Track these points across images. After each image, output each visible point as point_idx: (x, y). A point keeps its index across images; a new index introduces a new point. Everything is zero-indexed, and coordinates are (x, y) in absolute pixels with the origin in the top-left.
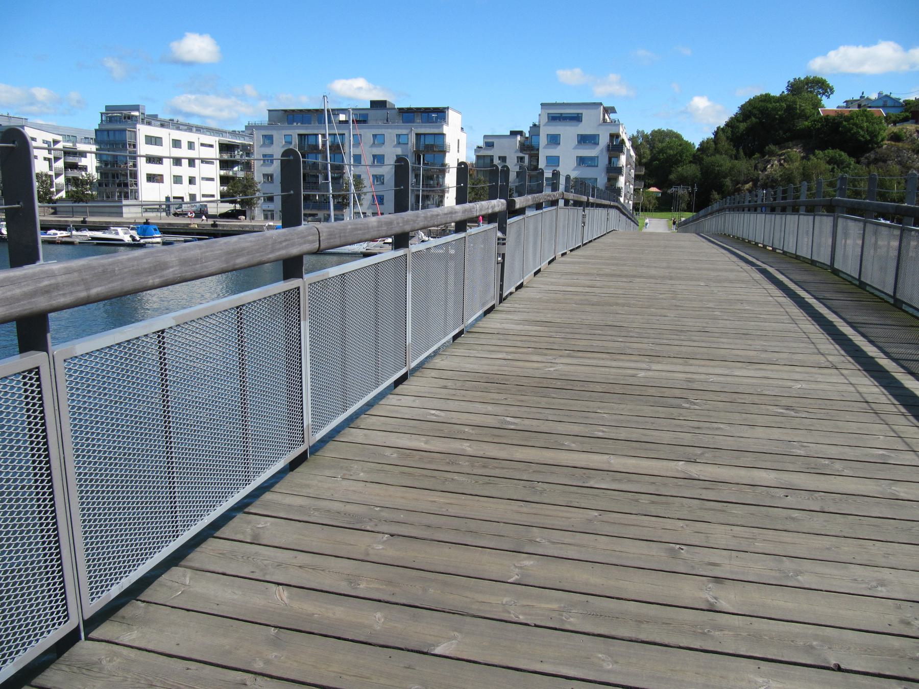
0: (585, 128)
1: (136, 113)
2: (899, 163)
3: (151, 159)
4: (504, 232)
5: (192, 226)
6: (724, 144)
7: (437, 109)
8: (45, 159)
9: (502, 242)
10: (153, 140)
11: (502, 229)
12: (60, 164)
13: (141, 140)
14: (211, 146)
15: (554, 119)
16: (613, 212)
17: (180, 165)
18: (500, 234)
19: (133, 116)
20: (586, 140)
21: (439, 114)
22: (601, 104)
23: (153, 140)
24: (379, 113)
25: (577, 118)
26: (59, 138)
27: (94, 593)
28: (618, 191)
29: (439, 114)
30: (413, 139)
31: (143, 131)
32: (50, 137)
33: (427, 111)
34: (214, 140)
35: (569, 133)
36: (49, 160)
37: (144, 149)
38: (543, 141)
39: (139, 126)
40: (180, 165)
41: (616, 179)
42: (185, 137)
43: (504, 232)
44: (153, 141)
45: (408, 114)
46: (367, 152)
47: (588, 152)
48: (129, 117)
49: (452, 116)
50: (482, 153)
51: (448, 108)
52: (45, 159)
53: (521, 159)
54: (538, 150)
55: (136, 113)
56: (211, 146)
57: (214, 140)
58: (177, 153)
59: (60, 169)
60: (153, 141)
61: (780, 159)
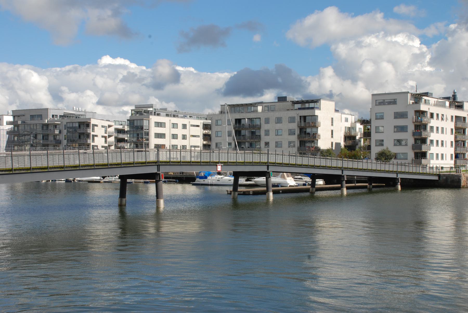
0: (398, 108)
1: (151, 109)
2: (389, 61)
3: (159, 136)
5: (170, 173)
6: (142, 125)
8: (103, 137)
10: (159, 124)
12: (112, 139)
13: (152, 124)
14: (198, 126)
19: (149, 111)
20: (400, 115)
22: (408, 92)
23: (159, 124)
24: (282, 104)
25: (394, 102)
26: (112, 124)
31: (154, 119)
32: (106, 124)
34: (200, 122)
35: (389, 111)
36: (105, 137)
37: (154, 130)
39: (151, 117)
42: (180, 121)
44: (159, 124)
47: (401, 122)
48: (148, 112)
52: (103, 137)
55: (151, 109)
56: (198, 126)
57: (200, 122)
58: (174, 131)
59: (112, 142)
60: (159, 124)
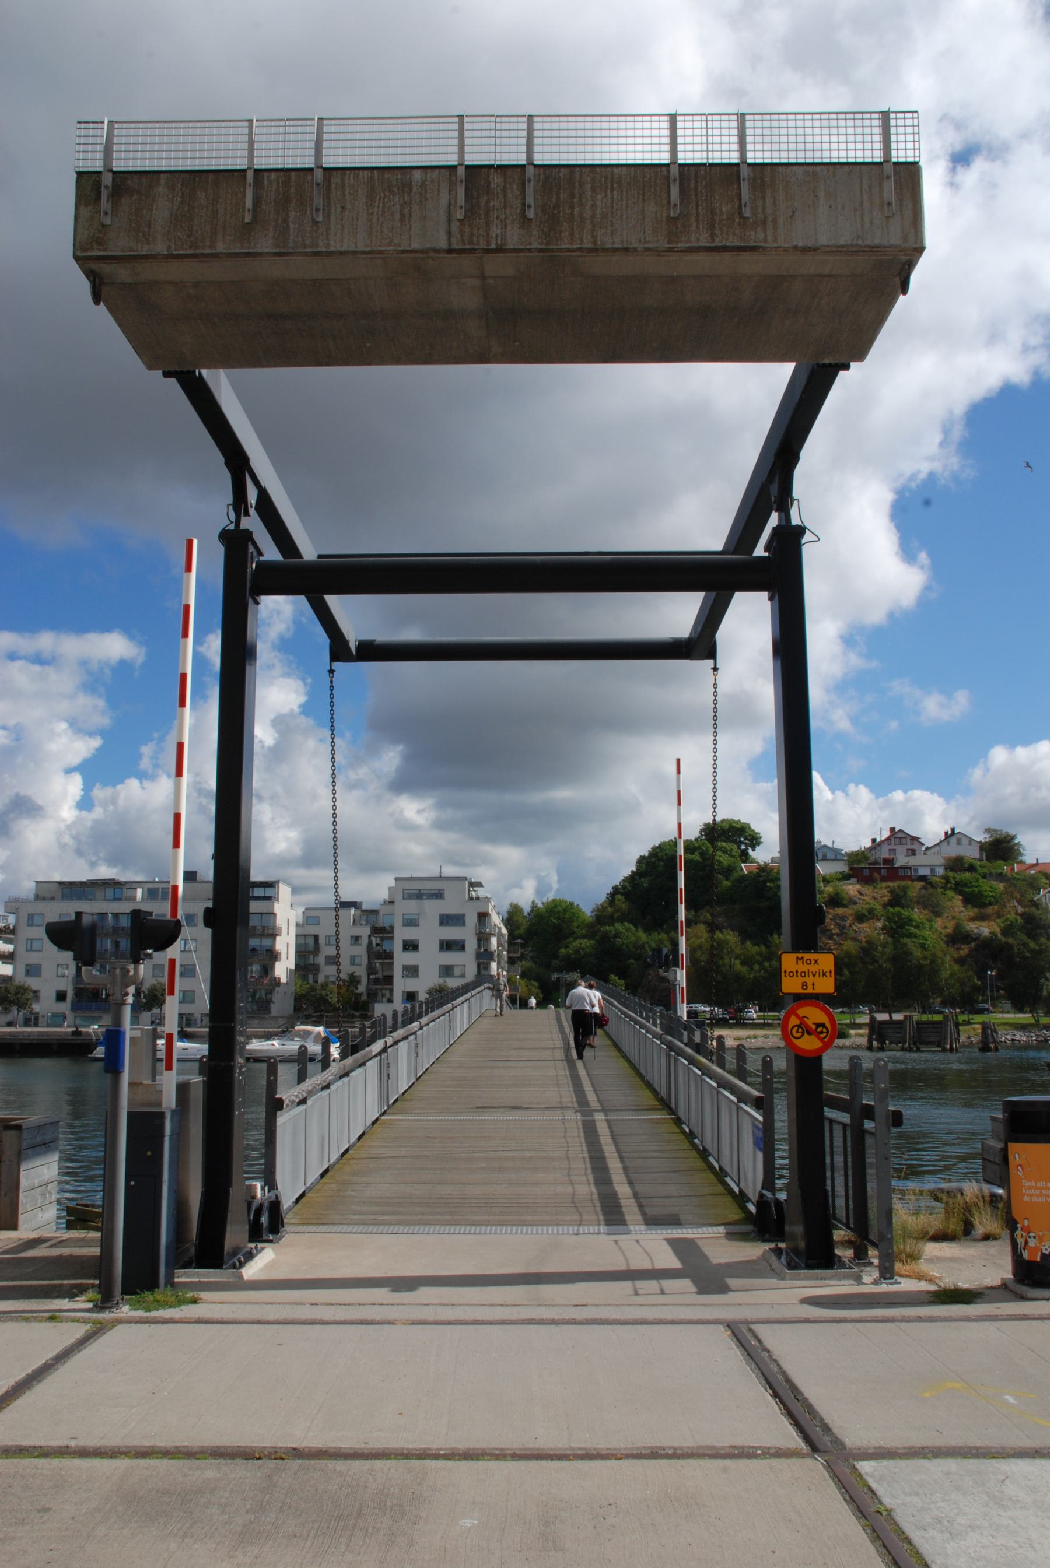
20: (446, 920)
22: (466, 879)
25: (438, 895)
35: (433, 909)
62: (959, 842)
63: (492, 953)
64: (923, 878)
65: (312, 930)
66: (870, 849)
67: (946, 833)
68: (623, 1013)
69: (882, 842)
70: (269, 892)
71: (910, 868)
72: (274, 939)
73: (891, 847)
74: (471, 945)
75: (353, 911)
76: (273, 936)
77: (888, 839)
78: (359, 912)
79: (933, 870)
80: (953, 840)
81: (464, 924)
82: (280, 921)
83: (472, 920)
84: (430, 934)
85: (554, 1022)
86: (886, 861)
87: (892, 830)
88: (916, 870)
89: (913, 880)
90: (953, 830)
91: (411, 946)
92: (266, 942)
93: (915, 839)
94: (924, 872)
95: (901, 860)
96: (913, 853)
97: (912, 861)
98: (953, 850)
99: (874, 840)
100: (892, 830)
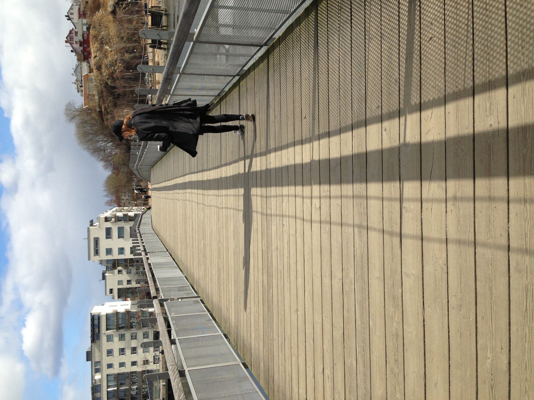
0: (102, 235)
4: (168, 299)
7: (91, 319)
9: (172, 299)
11: (166, 300)
15: (97, 252)
16: (143, 216)
17: (112, 341)
18: (169, 301)
20: (108, 232)
21: (95, 321)
22: (88, 228)
25: (97, 241)
27: (205, 312)
28: (136, 215)
29: (95, 321)
30: (110, 332)
33: (93, 325)
35: (104, 244)
38: (110, 257)
40: (112, 341)
41: (130, 217)
43: (168, 299)
45: (95, 337)
46: (116, 359)
49: (97, 310)
50: (116, 296)
51: (91, 314)
53: (120, 272)
54: (115, 260)
61: (139, 119)
62: (72, 14)
63: (124, 215)
64: (88, 29)
65: (116, 292)
66: (76, 52)
67: (68, 19)
68: (140, 160)
69: (73, 47)
70: (96, 318)
71: (83, 34)
72: (119, 313)
73: (75, 43)
74: (121, 224)
75: (106, 274)
76: (117, 313)
77: (71, 44)
78: (107, 272)
79: (84, 25)
80: (71, 16)
81: (110, 228)
82: (110, 311)
83: (108, 225)
84: (115, 243)
85: (163, 194)
86: (81, 45)
87: (66, 42)
88: (84, 32)
89: (89, 34)
90: (66, 16)
91: (121, 251)
92: (120, 316)
93: (71, 32)
94: (85, 29)
95: (79, 38)
96: (76, 33)
97: (80, 34)
98: (75, 16)
99: (72, 51)
100: (66, 42)
